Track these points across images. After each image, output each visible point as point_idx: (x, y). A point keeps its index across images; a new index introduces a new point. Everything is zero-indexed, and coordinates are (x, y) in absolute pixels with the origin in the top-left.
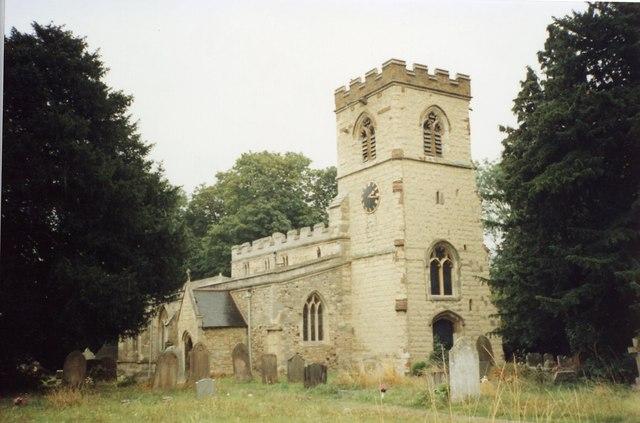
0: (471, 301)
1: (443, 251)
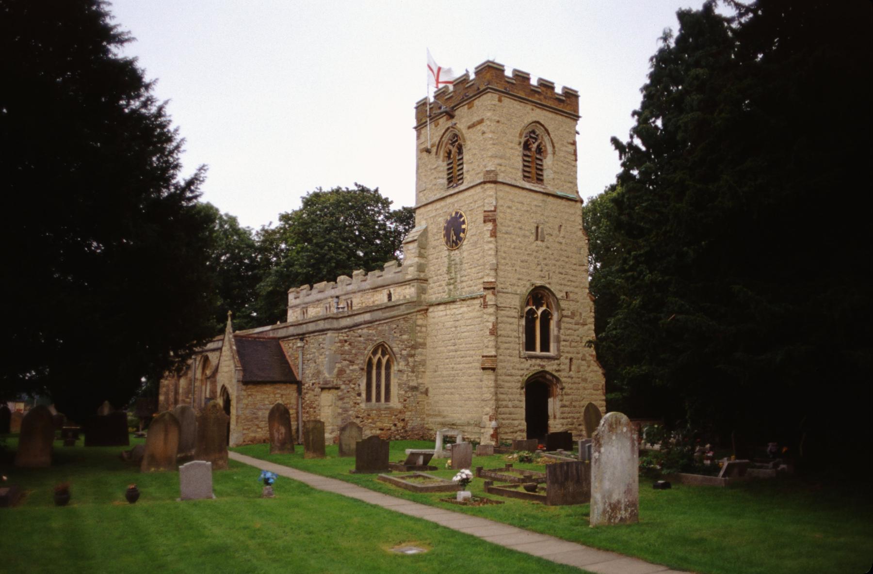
0: (571, 359)
1: (542, 298)
